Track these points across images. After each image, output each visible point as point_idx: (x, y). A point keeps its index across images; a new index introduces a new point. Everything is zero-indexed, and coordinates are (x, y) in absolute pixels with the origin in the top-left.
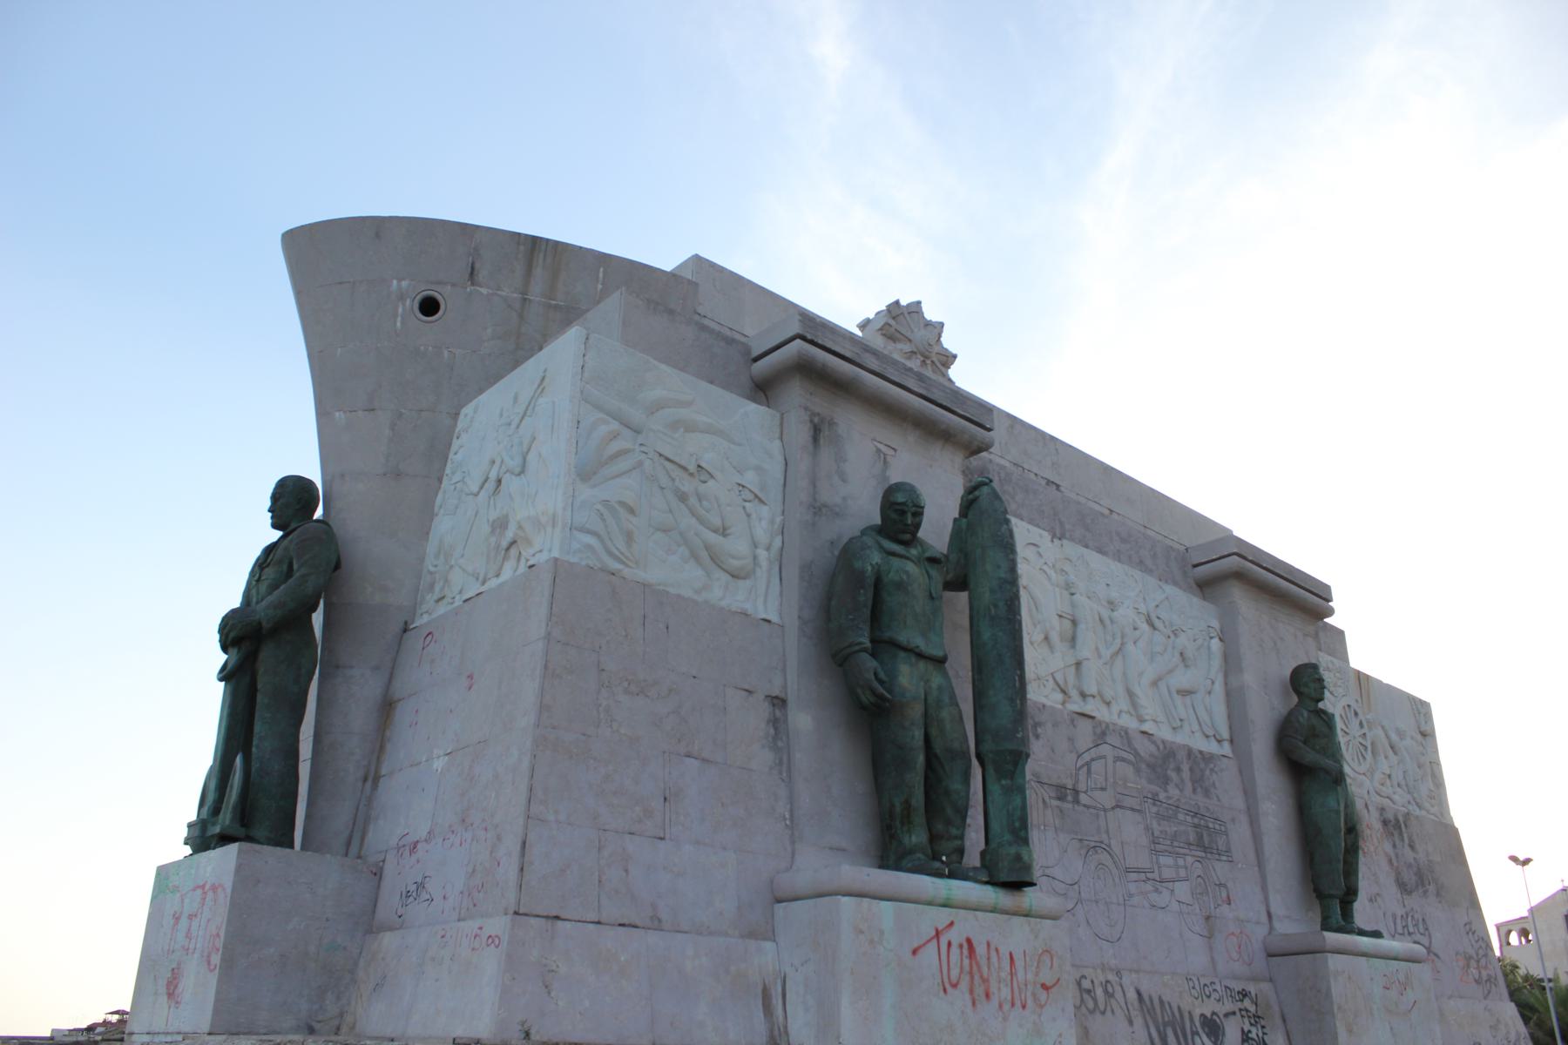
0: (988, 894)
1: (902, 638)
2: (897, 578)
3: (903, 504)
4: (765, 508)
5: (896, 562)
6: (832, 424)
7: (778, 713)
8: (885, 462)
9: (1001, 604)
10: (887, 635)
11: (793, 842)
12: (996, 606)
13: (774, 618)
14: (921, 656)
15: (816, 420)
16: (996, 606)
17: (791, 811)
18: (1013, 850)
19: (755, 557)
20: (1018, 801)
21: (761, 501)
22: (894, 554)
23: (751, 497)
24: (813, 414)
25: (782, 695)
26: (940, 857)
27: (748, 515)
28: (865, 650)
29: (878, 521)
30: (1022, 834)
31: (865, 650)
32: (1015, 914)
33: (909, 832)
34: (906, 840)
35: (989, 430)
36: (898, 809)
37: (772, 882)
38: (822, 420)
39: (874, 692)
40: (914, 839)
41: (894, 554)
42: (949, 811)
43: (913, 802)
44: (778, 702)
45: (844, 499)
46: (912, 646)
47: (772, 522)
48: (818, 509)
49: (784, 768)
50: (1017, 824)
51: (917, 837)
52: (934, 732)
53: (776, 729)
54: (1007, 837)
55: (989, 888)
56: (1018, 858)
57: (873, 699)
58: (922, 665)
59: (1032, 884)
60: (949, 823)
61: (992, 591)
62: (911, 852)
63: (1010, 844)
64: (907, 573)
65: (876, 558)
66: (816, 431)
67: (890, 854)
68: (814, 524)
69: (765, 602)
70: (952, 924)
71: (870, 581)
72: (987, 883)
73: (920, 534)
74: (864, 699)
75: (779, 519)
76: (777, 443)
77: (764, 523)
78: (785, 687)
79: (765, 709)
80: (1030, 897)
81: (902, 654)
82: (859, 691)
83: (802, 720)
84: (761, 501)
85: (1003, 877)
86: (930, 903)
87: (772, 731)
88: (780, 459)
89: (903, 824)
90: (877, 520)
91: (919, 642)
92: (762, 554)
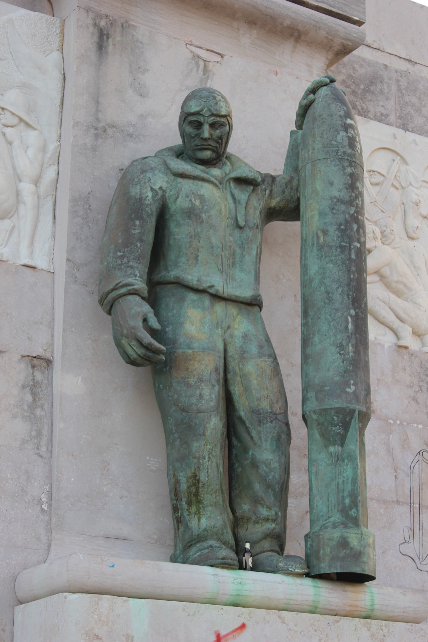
0: (308, 590)
1: (192, 277)
2: (187, 205)
3: (198, 113)
4: (33, 133)
5: (186, 185)
6: (126, 26)
7: (39, 376)
8: (206, 70)
9: (332, 229)
10: (173, 274)
11: (49, 530)
12: (325, 232)
13: (41, 263)
14: (217, 297)
15: (103, 23)
16: (325, 232)
17: (50, 493)
18: (337, 534)
19: (18, 194)
20: (349, 472)
21: (28, 125)
22: (183, 176)
23: (15, 121)
24: (99, 16)
25: (48, 355)
26: (244, 549)
27: (10, 143)
28: (135, 293)
29: (178, 141)
30: (353, 512)
31: (135, 293)
32: (349, 615)
33: (198, 513)
34: (194, 523)
35: (359, 23)
36: (184, 487)
37: (14, 580)
38: (112, 24)
39: (140, 343)
40: (204, 522)
41: (183, 176)
42: (257, 487)
43: (203, 477)
44: (41, 363)
45: (142, 117)
46: (205, 285)
47: (44, 149)
48: (100, 130)
49: (44, 442)
50: (347, 501)
51: (211, 518)
52: (236, 390)
53: (34, 395)
54: (337, 517)
55: (308, 581)
56: (344, 543)
57: (141, 351)
58: (220, 308)
59: (372, 578)
60: (256, 501)
61: (322, 214)
62: (200, 538)
63: (335, 526)
64: (201, 198)
65: (160, 181)
66: (102, 38)
67: (186, 548)
68: (94, 149)
69: (32, 244)
70: (243, 626)
71: (152, 209)
72: (300, 575)
73: (232, 148)
74: (130, 352)
75: (52, 146)
76: (56, 55)
77: (31, 152)
78: (51, 345)
79: (20, 372)
80: (365, 596)
81: (192, 296)
82: (124, 342)
83: (69, 384)
84: (28, 125)
85: (325, 568)
86: (212, 602)
87: (29, 398)
88: (57, 75)
89: (189, 503)
90: (177, 141)
91: (217, 282)
92: (27, 188)
